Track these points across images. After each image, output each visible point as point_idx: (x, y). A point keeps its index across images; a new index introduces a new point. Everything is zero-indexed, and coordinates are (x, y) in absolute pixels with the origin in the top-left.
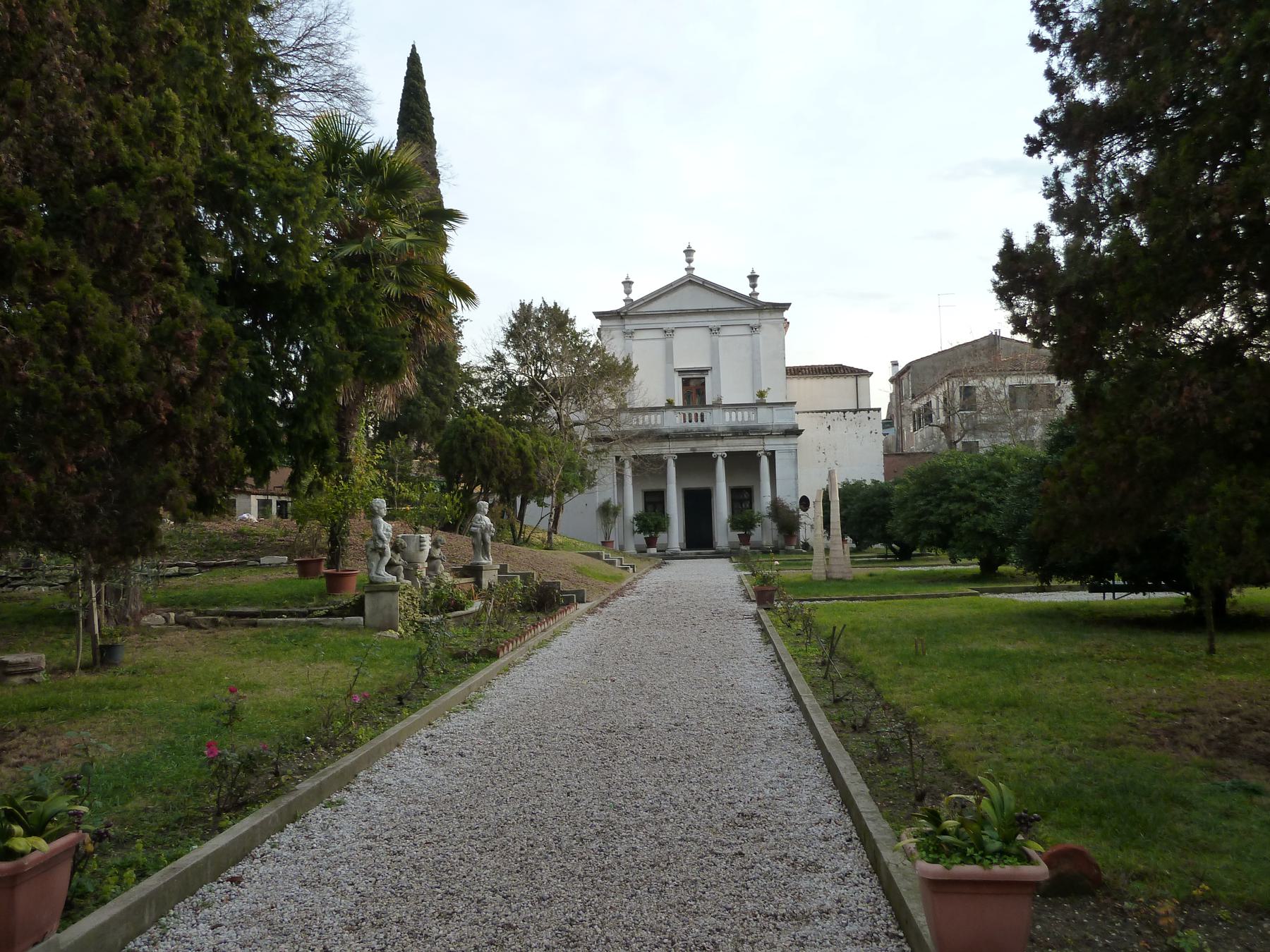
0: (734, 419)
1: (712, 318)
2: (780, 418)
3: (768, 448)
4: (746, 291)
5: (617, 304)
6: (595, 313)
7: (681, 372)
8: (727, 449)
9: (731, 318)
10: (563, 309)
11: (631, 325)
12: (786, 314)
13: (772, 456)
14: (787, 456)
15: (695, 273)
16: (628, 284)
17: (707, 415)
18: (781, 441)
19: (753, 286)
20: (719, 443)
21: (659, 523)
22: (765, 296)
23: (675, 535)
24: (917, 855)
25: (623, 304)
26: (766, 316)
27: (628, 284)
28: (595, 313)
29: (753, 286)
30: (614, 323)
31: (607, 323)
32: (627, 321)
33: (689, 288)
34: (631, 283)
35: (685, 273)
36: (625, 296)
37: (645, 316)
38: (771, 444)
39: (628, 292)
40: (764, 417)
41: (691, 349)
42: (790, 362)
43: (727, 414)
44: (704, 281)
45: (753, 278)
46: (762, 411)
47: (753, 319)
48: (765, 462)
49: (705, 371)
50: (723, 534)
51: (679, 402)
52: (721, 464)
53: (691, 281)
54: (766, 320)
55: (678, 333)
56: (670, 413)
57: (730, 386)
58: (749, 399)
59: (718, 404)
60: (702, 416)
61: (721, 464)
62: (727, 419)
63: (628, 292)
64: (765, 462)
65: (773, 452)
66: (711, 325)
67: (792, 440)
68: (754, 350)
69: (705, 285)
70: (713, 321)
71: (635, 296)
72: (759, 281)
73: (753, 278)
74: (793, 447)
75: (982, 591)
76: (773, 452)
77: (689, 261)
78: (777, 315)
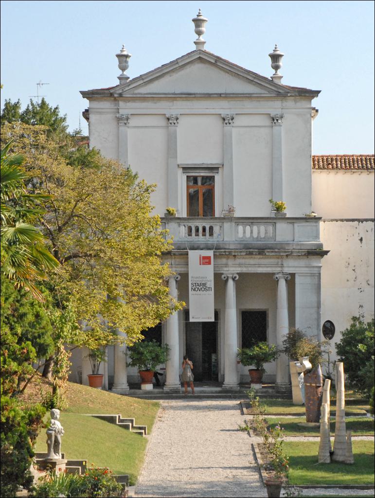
0: (248, 234)
1: (224, 104)
2: (301, 236)
3: (287, 270)
4: (267, 72)
5: (109, 80)
6: (81, 92)
7: (185, 169)
8: (239, 270)
9: (249, 106)
10: (52, 105)
11: (125, 108)
12: (315, 102)
13: (291, 281)
14: (308, 280)
15: (206, 48)
16: (123, 59)
17: (216, 229)
18: (303, 262)
19: (276, 68)
20: (231, 262)
21: (157, 356)
22: (289, 78)
23: (175, 366)
24: (243, 389)
25: (117, 82)
26: (290, 103)
27: (123, 59)
28: (81, 92)
29: (276, 68)
30: (106, 105)
31: (97, 105)
32: (121, 104)
33: (198, 67)
34: (127, 56)
35: (194, 48)
36: (120, 72)
37: (144, 98)
38: (291, 266)
39: (123, 68)
40: (283, 233)
41: (198, 140)
42: (318, 149)
43: (241, 228)
44: (218, 59)
45: (275, 58)
46: (281, 226)
47: (274, 107)
48: (282, 286)
49: (214, 169)
50: (230, 379)
51: (181, 209)
52: (231, 284)
53: (201, 58)
54: (290, 108)
55: (182, 121)
56: (172, 226)
57: (242, 195)
58: (266, 211)
59: (229, 218)
60: (211, 228)
61: (231, 284)
62: (241, 235)
63: (123, 68)
64: (282, 286)
65: (293, 275)
66: (224, 113)
67: (315, 262)
68: (274, 145)
69: (218, 63)
70: (224, 108)
71: (132, 73)
72: (281, 63)
73: (275, 58)
74: (315, 270)
75: (363, 418)
76: (293, 275)
77: (199, 33)
78: (303, 104)
